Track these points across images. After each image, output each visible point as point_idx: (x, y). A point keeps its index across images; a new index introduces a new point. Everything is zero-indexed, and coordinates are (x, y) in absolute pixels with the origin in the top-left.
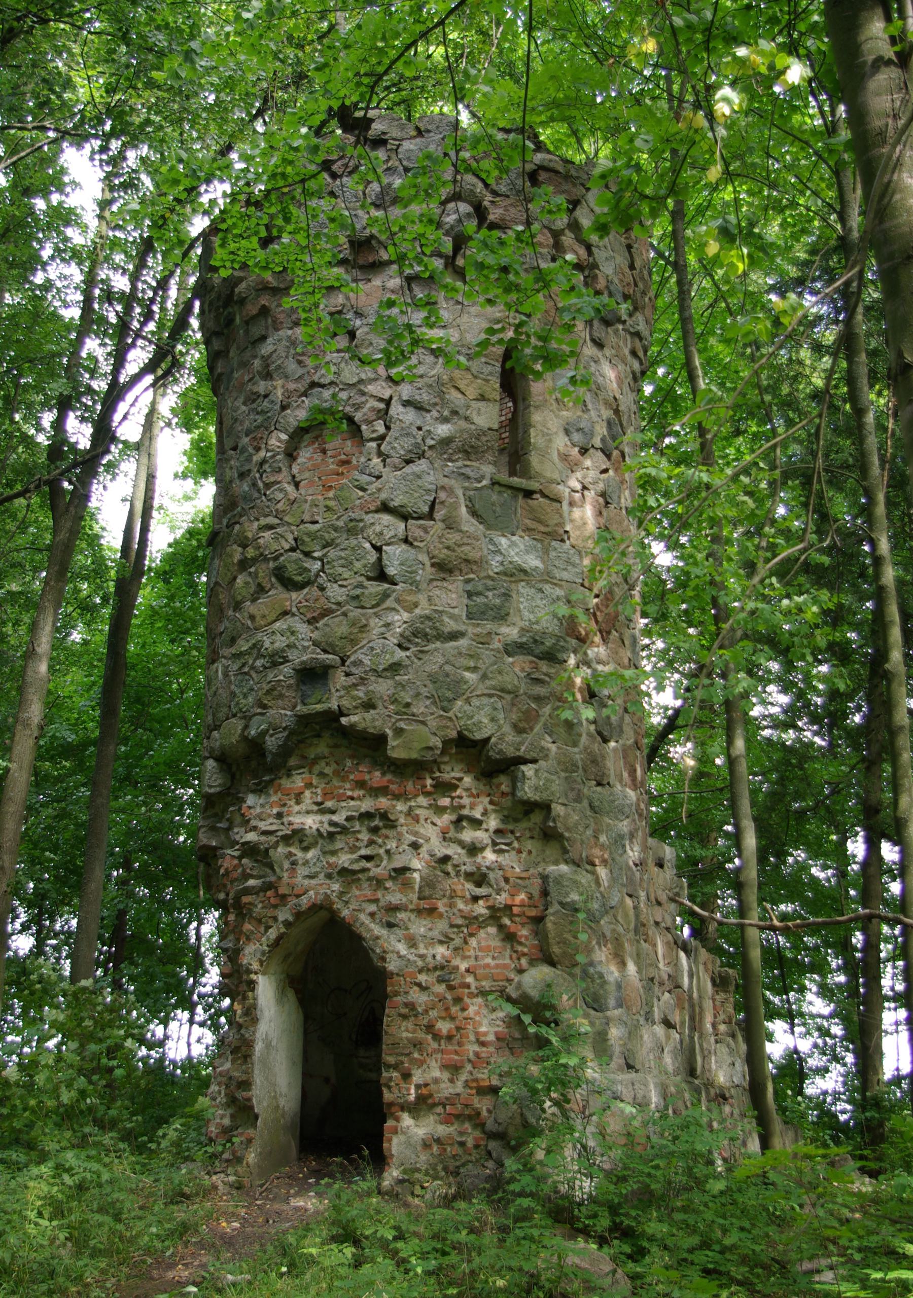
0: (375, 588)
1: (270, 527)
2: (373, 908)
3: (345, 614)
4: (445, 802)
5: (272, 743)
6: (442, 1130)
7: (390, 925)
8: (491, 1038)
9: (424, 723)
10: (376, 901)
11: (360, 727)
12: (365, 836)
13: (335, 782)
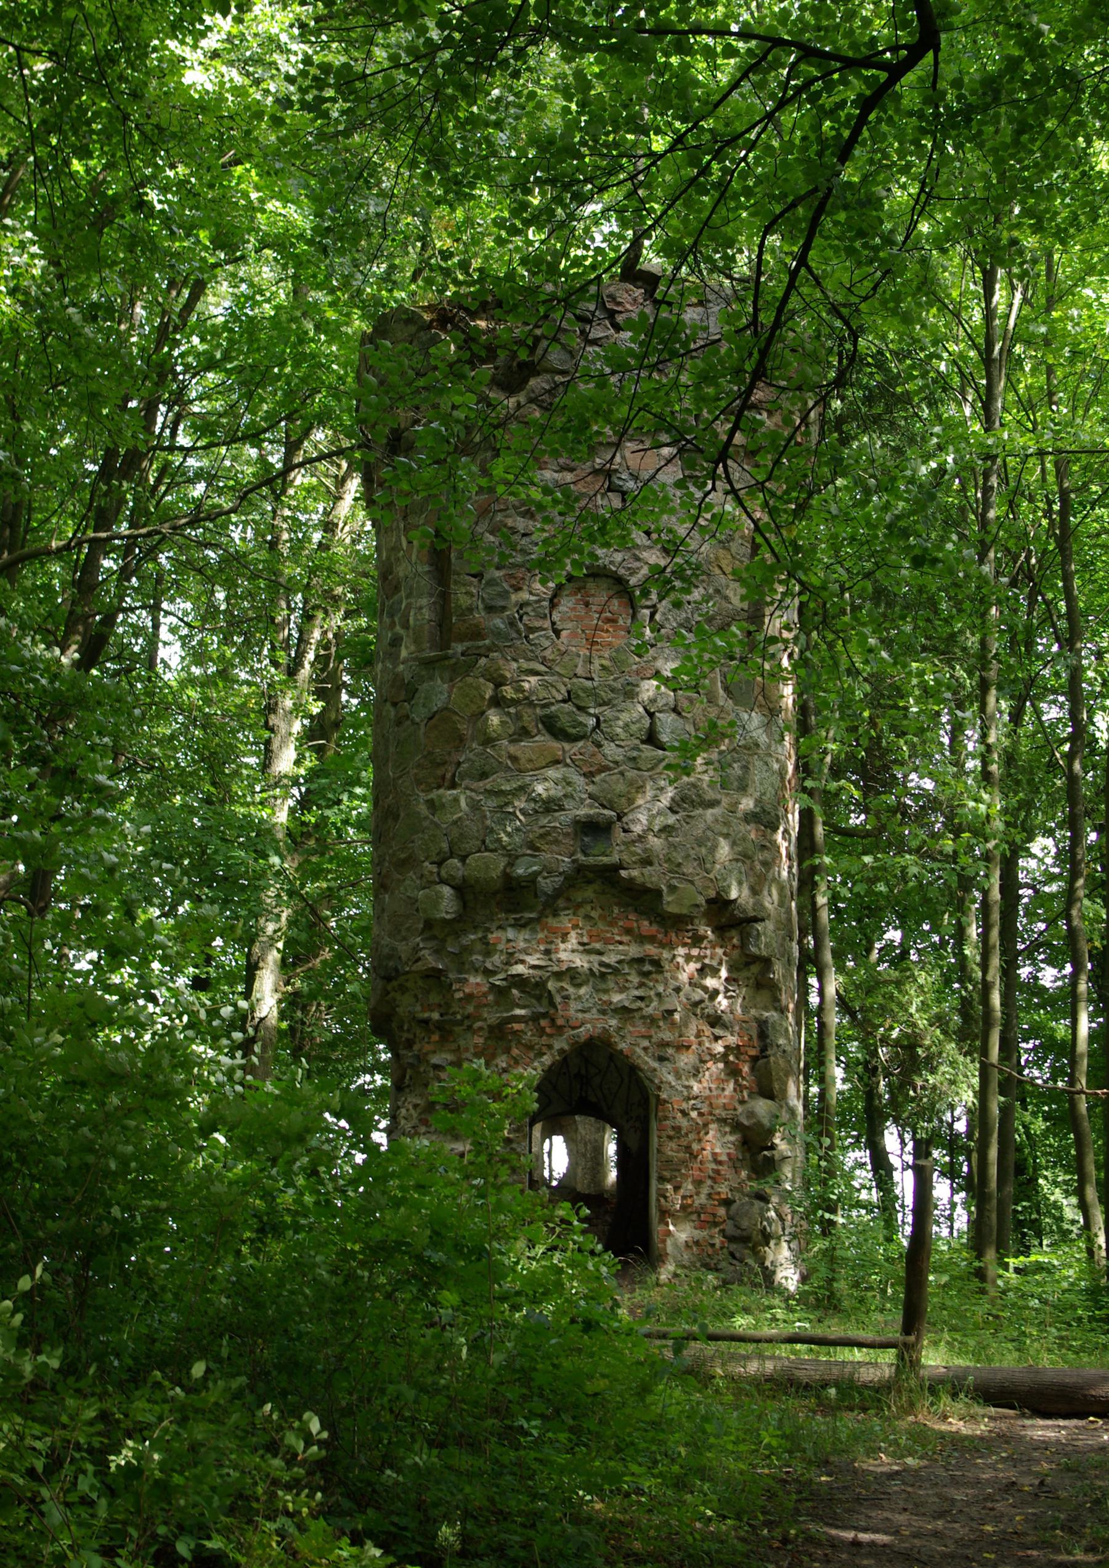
0: (648, 751)
1: (536, 673)
2: (646, 1043)
3: (622, 774)
4: (695, 952)
5: (547, 884)
6: (699, 1234)
7: (662, 1059)
8: (724, 1158)
9: (692, 882)
10: (649, 1037)
11: (640, 880)
12: (635, 979)
13: (601, 926)
